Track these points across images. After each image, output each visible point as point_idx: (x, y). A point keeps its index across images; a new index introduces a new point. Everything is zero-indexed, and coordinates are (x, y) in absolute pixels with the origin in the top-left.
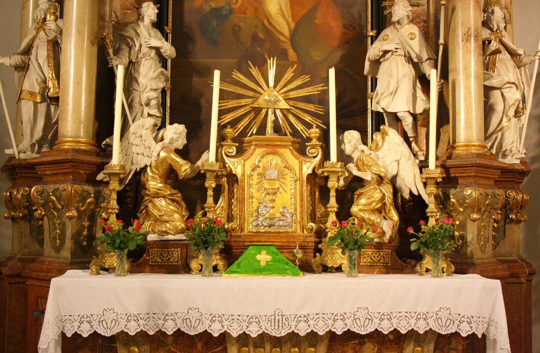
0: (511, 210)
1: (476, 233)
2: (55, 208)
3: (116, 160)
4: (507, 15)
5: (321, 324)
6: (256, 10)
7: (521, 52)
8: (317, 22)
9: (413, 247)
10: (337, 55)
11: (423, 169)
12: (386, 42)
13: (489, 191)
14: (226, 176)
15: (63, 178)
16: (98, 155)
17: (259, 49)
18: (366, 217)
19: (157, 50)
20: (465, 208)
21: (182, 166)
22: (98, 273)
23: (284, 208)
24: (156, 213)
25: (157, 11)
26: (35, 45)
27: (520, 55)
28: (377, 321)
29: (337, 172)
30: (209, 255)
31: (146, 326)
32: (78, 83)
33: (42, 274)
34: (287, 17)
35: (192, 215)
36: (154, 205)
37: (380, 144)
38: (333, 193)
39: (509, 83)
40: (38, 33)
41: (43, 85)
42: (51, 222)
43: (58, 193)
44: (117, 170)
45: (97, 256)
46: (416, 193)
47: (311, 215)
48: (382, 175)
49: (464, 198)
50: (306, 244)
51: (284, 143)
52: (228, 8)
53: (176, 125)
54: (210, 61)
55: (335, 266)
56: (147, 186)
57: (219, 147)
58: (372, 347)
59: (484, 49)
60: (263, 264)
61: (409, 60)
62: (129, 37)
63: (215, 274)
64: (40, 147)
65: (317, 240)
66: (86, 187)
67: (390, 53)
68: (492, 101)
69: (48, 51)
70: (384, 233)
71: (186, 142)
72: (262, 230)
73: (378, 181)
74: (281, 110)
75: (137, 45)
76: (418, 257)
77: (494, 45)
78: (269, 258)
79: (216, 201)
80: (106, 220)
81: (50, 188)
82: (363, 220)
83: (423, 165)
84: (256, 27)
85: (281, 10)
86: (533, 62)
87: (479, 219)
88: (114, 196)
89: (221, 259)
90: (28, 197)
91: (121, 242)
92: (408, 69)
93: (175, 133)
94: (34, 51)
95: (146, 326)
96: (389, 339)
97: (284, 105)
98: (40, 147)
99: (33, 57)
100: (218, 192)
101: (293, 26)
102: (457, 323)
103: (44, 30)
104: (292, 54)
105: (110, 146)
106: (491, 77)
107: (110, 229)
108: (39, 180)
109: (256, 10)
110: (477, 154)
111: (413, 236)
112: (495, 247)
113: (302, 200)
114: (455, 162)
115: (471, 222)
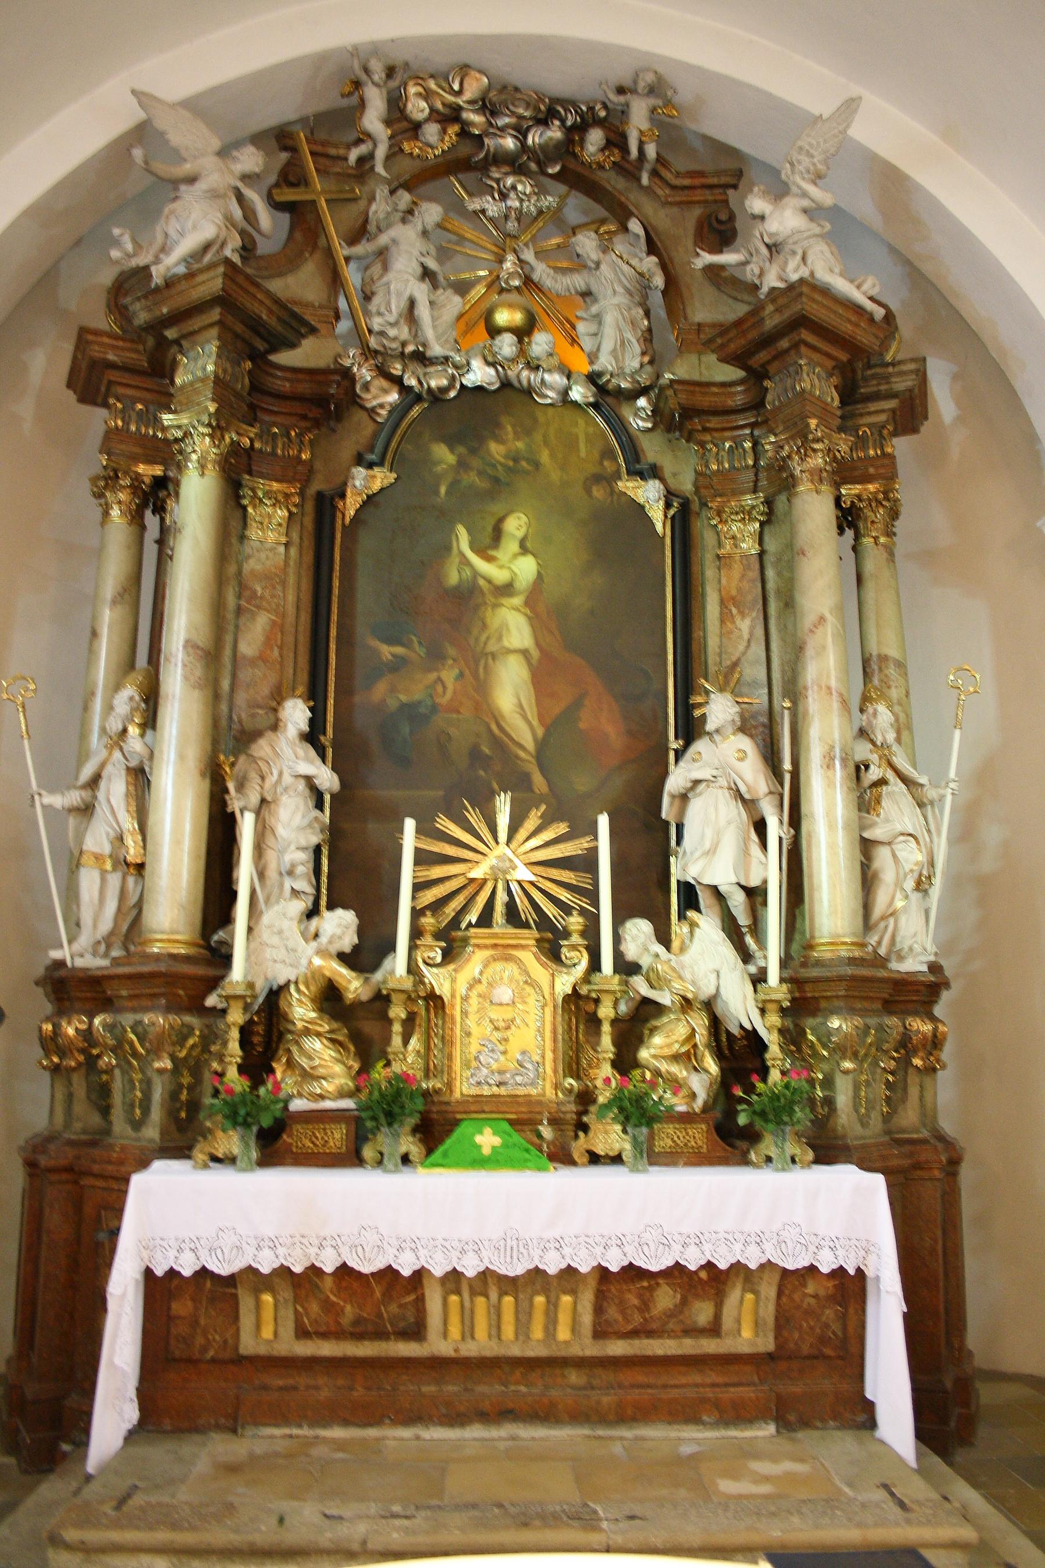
0: (915, 1052)
1: (850, 1093)
2: (135, 1054)
3: (238, 973)
4: (902, 716)
5: (583, 1253)
6: (477, 707)
7: (923, 780)
8: (582, 725)
9: (742, 1120)
10: (618, 783)
11: (759, 986)
12: (696, 764)
13: (872, 1021)
14: (425, 999)
15: (149, 1003)
16: (209, 963)
17: (482, 773)
18: (663, 1070)
19: (309, 780)
20: (832, 1051)
21: (350, 982)
22: (206, 1166)
23: (524, 1053)
24: (304, 1062)
25: (309, 714)
26: (104, 774)
27: (922, 785)
28: (677, 1247)
29: (614, 992)
30: (396, 1136)
31: (289, 1259)
32: (177, 842)
33: (110, 1167)
34: (530, 718)
35: (365, 1069)
36: (301, 1049)
37: (687, 941)
38: (606, 1028)
39: (903, 834)
40: (110, 754)
41: (117, 844)
42: (127, 1077)
43: (140, 1029)
44: (240, 991)
45: (205, 1137)
46: (748, 1026)
47: (570, 1066)
48: (690, 996)
49: (829, 1033)
50: (562, 1115)
51: (523, 942)
52: (429, 703)
53: (340, 912)
54: (397, 794)
55: (611, 1154)
56: (291, 1017)
57: (412, 948)
58: (671, 1292)
59: (858, 778)
60: (486, 1151)
61: (738, 795)
62: (261, 759)
63: (405, 1169)
64: (109, 946)
65: (581, 1108)
66: (188, 1019)
67: (704, 784)
68: (876, 864)
69: (128, 783)
70: (693, 1096)
71: (356, 941)
72: (486, 1091)
73: (682, 1005)
74: (519, 882)
75: (275, 773)
76: (752, 1136)
77: (874, 773)
78: (497, 1141)
79: (406, 1042)
80: (221, 1075)
81: (128, 1019)
82: (657, 1073)
83: (759, 979)
84: (478, 735)
85: (521, 706)
86: (942, 798)
87: (855, 1070)
88: (235, 1034)
89: (413, 1143)
90: (88, 1035)
91: (248, 1114)
92: (735, 812)
93: (339, 925)
94: (103, 784)
95: (289, 1259)
96: (699, 1278)
97: (524, 874)
98: (109, 946)
99: (101, 795)
100: (409, 1023)
101: (540, 732)
102: (812, 1248)
103: (121, 749)
104: (539, 781)
105: (230, 946)
106: (873, 825)
107: (230, 1091)
108: (106, 1004)
109: (477, 707)
110: (849, 958)
111: (741, 1100)
112: (887, 1118)
113: (555, 1040)
114: (814, 973)
115: (840, 1074)
